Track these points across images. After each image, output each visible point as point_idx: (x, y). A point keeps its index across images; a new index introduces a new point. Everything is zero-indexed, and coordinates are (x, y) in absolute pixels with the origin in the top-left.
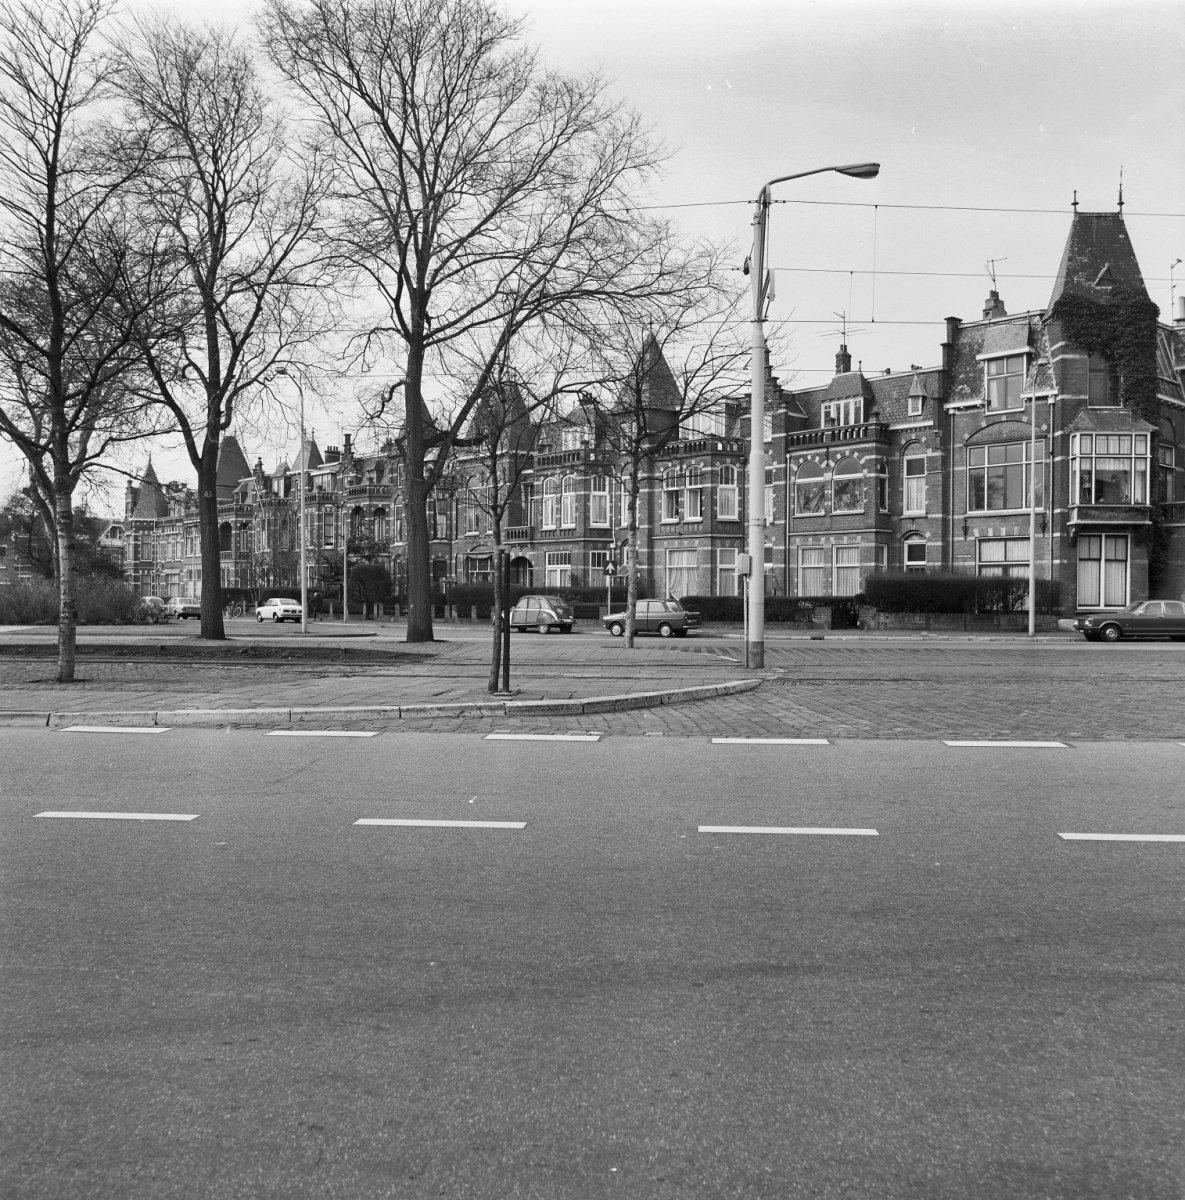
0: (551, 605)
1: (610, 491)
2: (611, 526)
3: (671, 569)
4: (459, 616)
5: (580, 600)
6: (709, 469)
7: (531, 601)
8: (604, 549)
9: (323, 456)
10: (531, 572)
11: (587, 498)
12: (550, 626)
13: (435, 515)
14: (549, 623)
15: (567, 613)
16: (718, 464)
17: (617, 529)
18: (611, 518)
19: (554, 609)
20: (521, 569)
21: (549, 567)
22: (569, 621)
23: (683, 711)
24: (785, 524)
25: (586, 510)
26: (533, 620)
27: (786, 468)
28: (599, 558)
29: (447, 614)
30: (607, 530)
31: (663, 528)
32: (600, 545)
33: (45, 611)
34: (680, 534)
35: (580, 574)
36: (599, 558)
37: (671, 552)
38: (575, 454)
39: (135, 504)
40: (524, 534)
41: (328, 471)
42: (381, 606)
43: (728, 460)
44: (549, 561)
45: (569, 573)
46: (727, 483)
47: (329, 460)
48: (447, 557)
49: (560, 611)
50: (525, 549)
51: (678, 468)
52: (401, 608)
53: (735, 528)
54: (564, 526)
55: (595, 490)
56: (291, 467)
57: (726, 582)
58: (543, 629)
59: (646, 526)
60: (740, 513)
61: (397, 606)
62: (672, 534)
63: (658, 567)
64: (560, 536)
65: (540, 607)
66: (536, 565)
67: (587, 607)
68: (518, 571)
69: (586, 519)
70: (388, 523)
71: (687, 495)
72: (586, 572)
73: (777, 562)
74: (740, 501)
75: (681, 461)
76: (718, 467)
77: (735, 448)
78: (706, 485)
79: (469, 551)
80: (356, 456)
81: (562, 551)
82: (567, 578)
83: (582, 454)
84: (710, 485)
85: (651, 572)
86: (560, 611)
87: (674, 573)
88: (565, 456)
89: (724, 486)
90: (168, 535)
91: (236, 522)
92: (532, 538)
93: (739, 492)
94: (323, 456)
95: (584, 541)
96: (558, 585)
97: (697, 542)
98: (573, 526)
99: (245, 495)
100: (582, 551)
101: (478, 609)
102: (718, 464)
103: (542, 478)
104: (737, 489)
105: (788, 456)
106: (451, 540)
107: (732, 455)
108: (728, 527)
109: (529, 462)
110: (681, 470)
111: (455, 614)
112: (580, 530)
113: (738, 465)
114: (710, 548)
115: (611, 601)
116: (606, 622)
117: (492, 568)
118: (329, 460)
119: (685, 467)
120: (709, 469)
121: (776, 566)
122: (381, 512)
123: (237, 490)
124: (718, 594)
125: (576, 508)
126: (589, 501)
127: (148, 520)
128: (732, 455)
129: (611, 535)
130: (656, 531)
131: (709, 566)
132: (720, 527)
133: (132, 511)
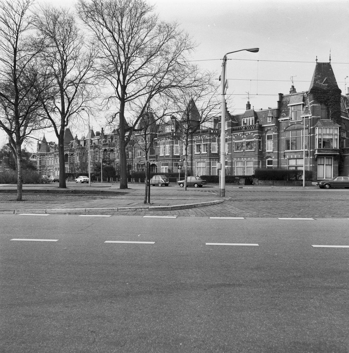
0: (162, 178)
1: (180, 144)
2: (180, 155)
3: (198, 167)
4: (135, 181)
5: (171, 176)
6: (209, 138)
7: (156, 177)
8: (178, 161)
9: (95, 134)
10: (156, 168)
11: (173, 146)
12: (162, 184)
13: (128, 151)
14: (162, 183)
15: (167, 180)
16: (211, 136)
17: (182, 155)
18: (180, 152)
19: (163, 179)
20: (153, 167)
21: (162, 167)
22: (168, 183)
23: (201, 209)
24: (231, 154)
25: (173, 150)
26: (157, 182)
27: (232, 138)
28: (176, 164)
29: (132, 180)
30: (179, 156)
31: (195, 155)
32: (177, 160)
33: (13, 180)
34: (200, 157)
35: (171, 169)
36: (176, 164)
37: (197, 162)
38: (169, 134)
39: (40, 148)
40: (154, 157)
41: (97, 139)
42: (112, 178)
43: (215, 135)
44: (162, 165)
45: (168, 169)
46: (214, 142)
47: (97, 135)
48: (132, 164)
49: (165, 180)
50: (155, 161)
51: (200, 138)
52: (118, 179)
53: (217, 155)
54: (166, 155)
55: (175, 144)
56: (86, 137)
57: (214, 171)
58: (160, 185)
59: (190, 155)
60: (218, 151)
61: (117, 178)
62: (198, 157)
63: (194, 167)
64: (165, 158)
65: (159, 179)
66: (158, 166)
67: (173, 179)
68: (153, 168)
69: (173, 153)
70: (114, 154)
71: (202, 146)
72: (172, 168)
73: (229, 165)
74: (218, 147)
75: (201, 136)
76: (212, 137)
77: (216, 132)
78: (208, 143)
79: (138, 162)
80: (105, 134)
81: (166, 162)
82: (167, 170)
83: (171, 134)
84: (209, 143)
85: (192, 168)
86: (165, 180)
87: (199, 169)
89: (213, 143)
90: (49, 157)
91: (70, 153)
92: (157, 158)
93: (218, 145)
94: (95, 134)
95: (172, 159)
96: (164, 172)
97: (205, 159)
98: (169, 155)
99: (72, 146)
100: (171, 162)
101: (141, 179)
102: (211, 136)
103: (160, 141)
104: (217, 144)
105: (232, 134)
106: (133, 159)
107: (215, 134)
108: (214, 155)
109: (156, 136)
110: (201, 138)
111: (134, 181)
112: (171, 156)
113: (217, 137)
114: (209, 161)
115: (180, 177)
116: (179, 183)
117: (145, 167)
118: (97, 135)
119: (202, 137)
120: (209, 138)
121: (229, 166)
123: (70, 144)
124: (211, 175)
125: (170, 149)
126: (173, 147)
127: (44, 153)
128: (215, 134)
129: (180, 157)
130: (193, 156)
131: (209, 166)
132: (212, 155)
133: (39, 150)
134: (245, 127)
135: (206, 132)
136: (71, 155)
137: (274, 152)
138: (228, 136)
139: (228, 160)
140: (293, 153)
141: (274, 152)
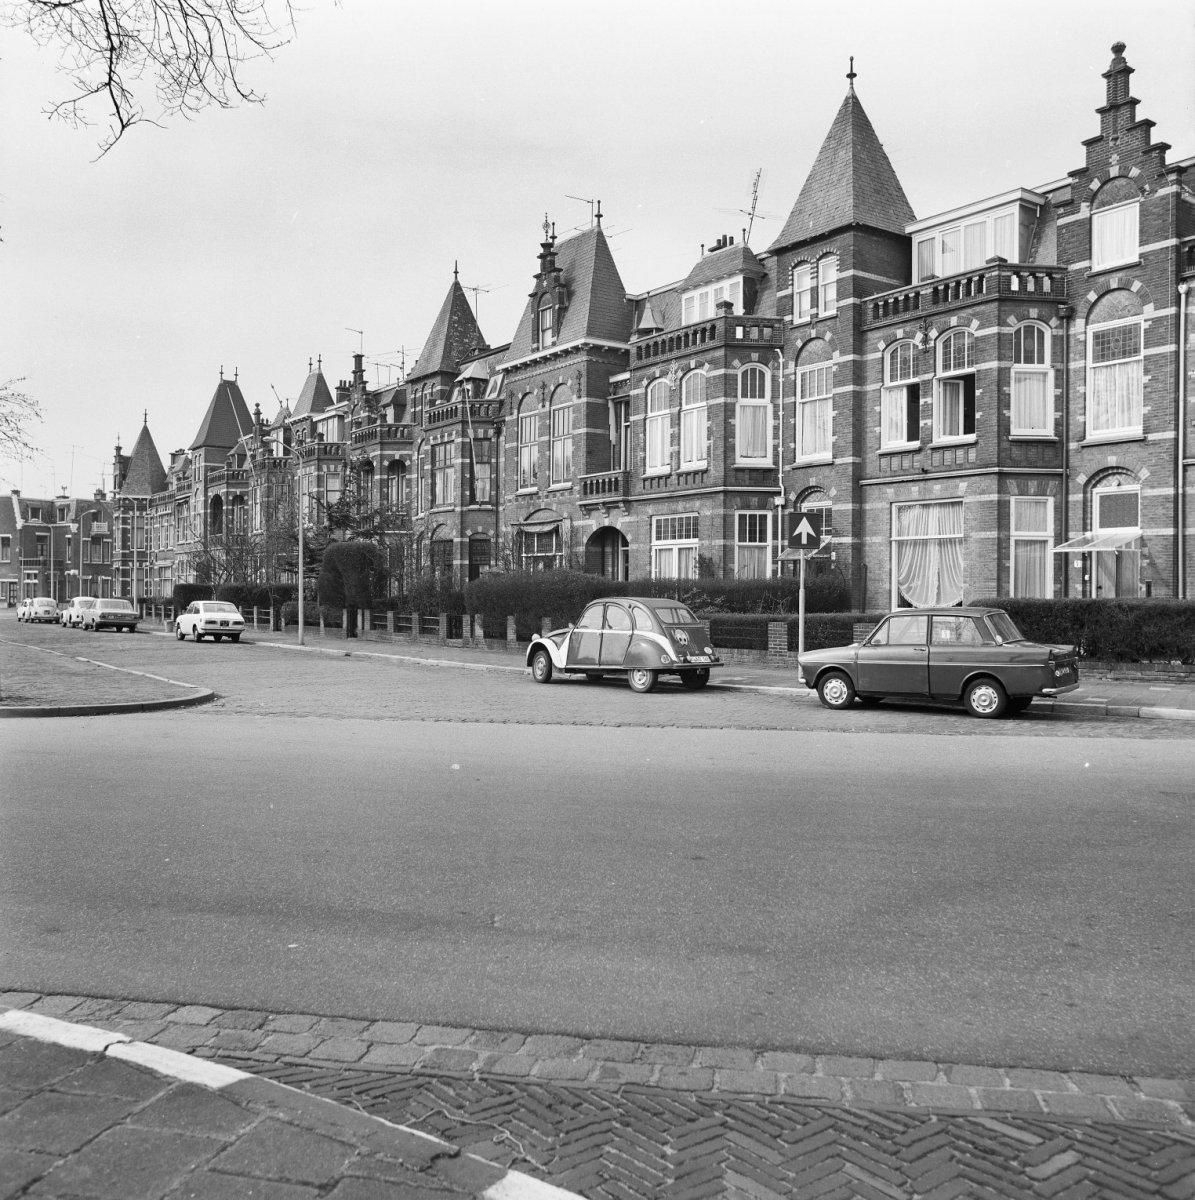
0: (659, 622)
1: (774, 397)
2: (776, 463)
3: (900, 544)
4: (487, 635)
5: (721, 607)
6: (994, 330)
7: (612, 611)
8: (763, 507)
9: (334, 394)
10: (626, 554)
11: (729, 411)
12: (656, 672)
13: (471, 463)
14: (655, 664)
15: (698, 640)
16: (1012, 319)
17: (788, 468)
18: (775, 448)
19: (667, 630)
20: (608, 550)
21: (657, 544)
22: (703, 660)
24: (1176, 440)
25: (729, 433)
26: (614, 656)
27: (1177, 316)
28: (753, 525)
29: (466, 630)
30: (769, 470)
31: (884, 461)
32: (755, 500)
33: (392, 604)
34: (925, 471)
35: (716, 556)
36: (753, 525)
37: (900, 509)
38: (706, 330)
39: (123, 476)
40: (613, 486)
41: (333, 413)
42: (367, 613)
43: (1034, 312)
44: (658, 532)
45: (694, 555)
46: (1029, 360)
47: (341, 399)
48: (491, 532)
49: (680, 635)
50: (614, 512)
51: (919, 336)
52: (397, 619)
53: (1049, 453)
54: (685, 467)
55: (744, 395)
56: (292, 410)
57: (1028, 576)
58: (639, 680)
59: (850, 460)
60: (1058, 423)
61: (390, 615)
62: (905, 472)
63: (874, 541)
64: (681, 485)
65: (634, 627)
66: (636, 540)
67: (741, 623)
68: (603, 554)
69: (729, 450)
70: (409, 485)
71: (937, 390)
72: (727, 551)
73: (1152, 521)
74: (1058, 398)
75: (925, 321)
76: (1013, 325)
77: (1047, 284)
78: (984, 366)
79: (522, 521)
80: (370, 388)
81: (683, 511)
82: (692, 563)
83: (720, 326)
84: (994, 364)
85: (858, 549)
86: (680, 635)
87: (908, 552)
88: (687, 335)
89: (1022, 367)
90: (162, 516)
91: (227, 493)
92: (627, 493)
93: (1056, 379)
94: (334, 394)
95: (724, 492)
96: (675, 575)
97: (963, 485)
98: (703, 465)
99: (242, 457)
100: (721, 511)
101: (517, 622)
102: (1012, 319)
103: (645, 382)
104: (1051, 374)
105: (1183, 288)
106: (497, 504)
107: (1038, 299)
108: (1033, 452)
109: (621, 360)
110: (925, 340)
111: (479, 632)
112: (717, 472)
113: (1054, 322)
114: (995, 497)
115: (807, 610)
116: (807, 670)
117: (559, 548)
118: (341, 399)
119: (933, 334)
120: (994, 330)
121: (1150, 532)
122: (398, 467)
123: (232, 452)
124: (1012, 595)
125: (709, 429)
126: (733, 416)
127: (140, 497)
128: (1038, 299)
129: (776, 480)
130: (870, 469)
131: (994, 534)
132: (1016, 452)
133: (120, 486)
134: (936, 290)
135: (906, 309)
136: (233, 503)
137: (1151, 437)
138: (836, 354)
139: (836, 500)
140: (1135, 444)
141: (1151, 437)
